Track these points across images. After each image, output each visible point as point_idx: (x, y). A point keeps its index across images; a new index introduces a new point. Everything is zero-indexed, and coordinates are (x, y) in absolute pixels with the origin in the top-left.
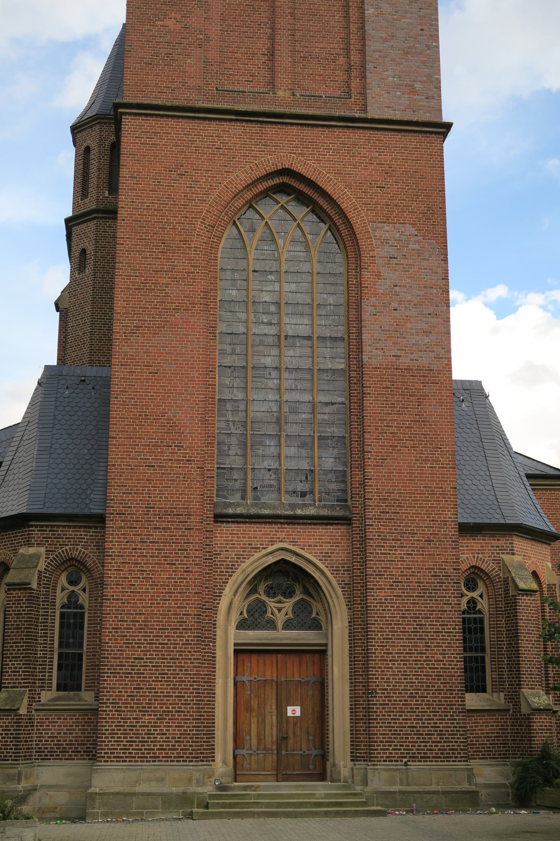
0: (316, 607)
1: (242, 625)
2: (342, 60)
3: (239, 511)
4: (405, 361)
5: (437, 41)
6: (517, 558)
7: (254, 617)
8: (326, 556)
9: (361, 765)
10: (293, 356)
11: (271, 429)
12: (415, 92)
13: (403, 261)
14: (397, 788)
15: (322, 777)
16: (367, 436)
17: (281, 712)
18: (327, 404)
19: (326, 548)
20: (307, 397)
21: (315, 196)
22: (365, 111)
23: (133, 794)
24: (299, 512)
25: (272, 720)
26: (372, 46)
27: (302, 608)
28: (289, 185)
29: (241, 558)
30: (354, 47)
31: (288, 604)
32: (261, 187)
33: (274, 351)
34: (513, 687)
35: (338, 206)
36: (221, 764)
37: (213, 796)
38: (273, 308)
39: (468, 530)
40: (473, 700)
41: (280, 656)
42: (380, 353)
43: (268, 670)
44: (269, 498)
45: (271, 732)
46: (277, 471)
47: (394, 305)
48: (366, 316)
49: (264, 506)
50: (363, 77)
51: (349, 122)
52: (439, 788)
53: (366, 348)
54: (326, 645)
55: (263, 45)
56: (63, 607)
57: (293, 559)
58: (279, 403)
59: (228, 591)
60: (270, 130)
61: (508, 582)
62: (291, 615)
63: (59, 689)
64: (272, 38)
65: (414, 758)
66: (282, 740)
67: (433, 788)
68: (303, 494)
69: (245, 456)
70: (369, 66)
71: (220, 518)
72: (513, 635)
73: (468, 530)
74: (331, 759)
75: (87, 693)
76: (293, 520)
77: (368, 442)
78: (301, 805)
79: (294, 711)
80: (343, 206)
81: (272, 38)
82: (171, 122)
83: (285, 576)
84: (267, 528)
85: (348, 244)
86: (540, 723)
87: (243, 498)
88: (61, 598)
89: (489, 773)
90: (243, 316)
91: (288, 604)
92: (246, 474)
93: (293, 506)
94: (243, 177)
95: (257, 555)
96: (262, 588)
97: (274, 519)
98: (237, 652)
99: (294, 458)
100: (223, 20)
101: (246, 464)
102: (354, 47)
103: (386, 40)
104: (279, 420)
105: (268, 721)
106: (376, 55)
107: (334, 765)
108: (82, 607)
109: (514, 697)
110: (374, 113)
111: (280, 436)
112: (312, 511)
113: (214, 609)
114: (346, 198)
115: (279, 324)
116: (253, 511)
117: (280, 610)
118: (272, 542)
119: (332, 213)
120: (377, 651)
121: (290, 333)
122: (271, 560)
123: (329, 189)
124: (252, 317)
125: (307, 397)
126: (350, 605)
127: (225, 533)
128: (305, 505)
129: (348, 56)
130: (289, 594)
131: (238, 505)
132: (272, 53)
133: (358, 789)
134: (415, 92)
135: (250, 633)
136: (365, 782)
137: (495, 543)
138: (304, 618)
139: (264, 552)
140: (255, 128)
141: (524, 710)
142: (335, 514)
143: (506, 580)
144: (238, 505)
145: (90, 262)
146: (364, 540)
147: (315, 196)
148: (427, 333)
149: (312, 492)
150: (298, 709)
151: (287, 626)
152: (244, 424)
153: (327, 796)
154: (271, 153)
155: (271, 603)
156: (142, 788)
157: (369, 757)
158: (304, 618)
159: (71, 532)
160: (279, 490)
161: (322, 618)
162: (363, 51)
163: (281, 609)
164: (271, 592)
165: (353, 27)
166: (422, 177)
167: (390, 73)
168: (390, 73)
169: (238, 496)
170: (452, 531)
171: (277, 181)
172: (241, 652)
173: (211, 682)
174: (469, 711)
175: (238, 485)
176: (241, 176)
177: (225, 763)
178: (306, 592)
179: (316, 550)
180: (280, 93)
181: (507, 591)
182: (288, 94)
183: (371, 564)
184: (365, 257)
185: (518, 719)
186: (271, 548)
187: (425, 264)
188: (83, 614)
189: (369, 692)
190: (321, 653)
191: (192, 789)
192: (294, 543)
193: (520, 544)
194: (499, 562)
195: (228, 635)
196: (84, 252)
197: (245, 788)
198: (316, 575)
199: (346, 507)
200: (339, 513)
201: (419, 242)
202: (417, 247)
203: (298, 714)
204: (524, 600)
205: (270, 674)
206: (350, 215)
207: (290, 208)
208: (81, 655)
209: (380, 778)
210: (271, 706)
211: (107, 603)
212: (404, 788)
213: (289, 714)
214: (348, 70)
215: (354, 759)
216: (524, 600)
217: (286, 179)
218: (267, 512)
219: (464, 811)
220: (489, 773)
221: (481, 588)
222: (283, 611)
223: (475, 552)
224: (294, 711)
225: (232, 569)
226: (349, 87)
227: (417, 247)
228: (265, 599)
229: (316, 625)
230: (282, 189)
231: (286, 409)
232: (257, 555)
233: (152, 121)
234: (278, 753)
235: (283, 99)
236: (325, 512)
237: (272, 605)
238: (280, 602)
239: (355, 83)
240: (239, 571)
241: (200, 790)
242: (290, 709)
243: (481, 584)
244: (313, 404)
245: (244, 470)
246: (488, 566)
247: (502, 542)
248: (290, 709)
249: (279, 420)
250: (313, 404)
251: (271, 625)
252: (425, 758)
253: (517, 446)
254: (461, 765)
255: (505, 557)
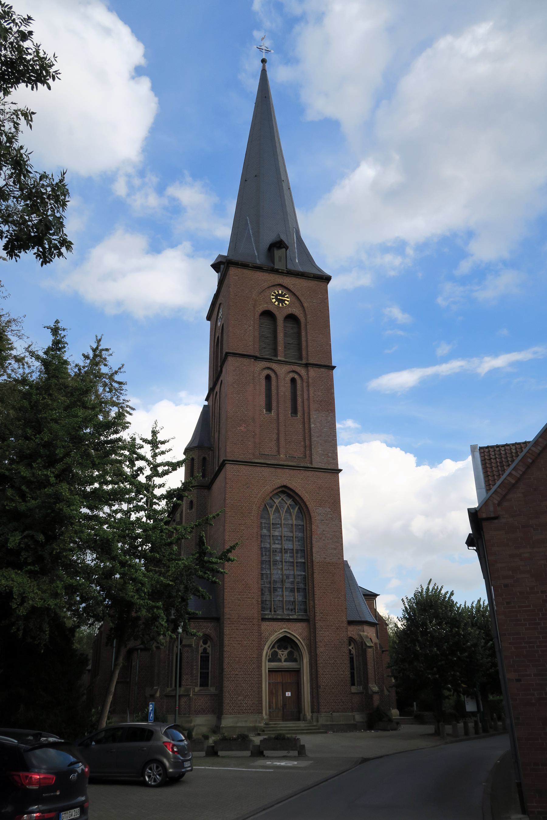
0: (296, 655)
1: (270, 661)
2: (302, 443)
3: (270, 617)
4: (328, 560)
5: (336, 437)
6: (365, 633)
7: (274, 658)
8: (300, 634)
9: (315, 714)
10: (287, 557)
11: (279, 585)
12: (329, 457)
13: (326, 522)
14: (329, 723)
15: (299, 719)
16: (315, 588)
17: (284, 694)
18: (299, 575)
19: (300, 631)
20: (292, 573)
21: (294, 495)
22: (311, 463)
23: (237, 727)
24: (291, 617)
25: (280, 698)
26: (314, 439)
27: (290, 654)
28: (286, 491)
29: (271, 635)
30: (307, 439)
31: (286, 652)
32: (275, 492)
33: (280, 554)
34: (365, 683)
35: (303, 500)
36: (265, 714)
37: (264, 727)
38: (279, 538)
39: (350, 623)
40: (354, 689)
41: (283, 673)
42: (319, 556)
43: (279, 678)
44: (279, 612)
45: (280, 703)
46: (282, 601)
47: (323, 538)
48: (314, 542)
49: (278, 615)
50: (311, 450)
51: (306, 468)
52: (343, 723)
53: (314, 555)
54: (300, 668)
55: (275, 436)
56: (201, 653)
57: (289, 635)
58: (282, 575)
59: (266, 647)
60: (279, 470)
61: (363, 643)
62: (287, 657)
63: (200, 686)
64: (278, 434)
65: (334, 712)
66: (284, 706)
67: (341, 723)
68: (292, 610)
69: (271, 595)
70: (313, 447)
71: (263, 619)
72: (365, 663)
73: (350, 623)
74: (303, 712)
75: (212, 688)
76: (289, 620)
77: (315, 591)
78: (297, 730)
79: (288, 694)
80: (305, 500)
81: (278, 434)
82: (244, 467)
83: (285, 642)
84: (279, 623)
85: (306, 514)
86: (376, 698)
87: (270, 611)
88: (201, 650)
89: (359, 717)
90: (268, 541)
91: (286, 652)
92: (271, 602)
93: (289, 615)
94: (269, 488)
95: (276, 634)
96: (276, 646)
97: (282, 620)
98: (269, 671)
99: (288, 596)
100: (260, 427)
101: (271, 598)
102: (307, 439)
103: (318, 437)
104: (282, 581)
105: (279, 697)
106: (315, 442)
107: (305, 715)
108: (208, 653)
109: (366, 687)
110: (315, 465)
111: (283, 588)
112: (295, 617)
113: (261, 655)
114: (306, 497)
115: (282, 544)
116: (275, 617)
117: (283, 654)
118: (281, 629)
119: (300, 502)
120: (320, 671)
121: (286, 548)
122: (281, 636)
123: (300, 493)
124: (272, 542)
125: (292, 573)
126: (310, 653)
127: (265, 625)
128: (292, 615)
129: (305, 442)
130: (286, 648)
131: (269, 614)
132: (278, 439)
133: (315, 723)
134: (329, 457)
135: (272, 664)
136: (318, 721)
137: (357, 628)
138: (291, 658)
139: (279, 633)
140: (273, 470)
141: (370, 692)
142: (304, 618)
143: (362, 642)
144: (269, 614)
145: (195, 506)
146: (315, 628)
147: (294, 495)
148: (335, 549)
149: (295, 609)
150: (290, 693)
151: (285, 661)
152: (270, 583)
153: (305, 726)
154: (279, 479)
155: (280, 652)
156: (239, 724)
157: (318, 711)
158: (291, 658)
159: (205, 624)
160: (283, 608)
161: (298, 658)
162: (310, 440)
163: (283, 654)
164: (279, 648)
165: (307, 431)
166: (332, 489)
167: (320, 449)
168: (320, 449)
169: (269, 610)
170: (345, 624)
171: (281, 489)
172: (271, 671)
173: (261, 683)
174: (352, 693)
175: (268, 606)
176: (269, 488)
177: (266, 714)
178: (292, 647)
179: (297, 632)
180: (282, 456)
181: (362, 647)
182: (284, 456)
183: (317, 638)
184: (313, 520)
185: (367, 695)
186: (281, 631)
187: (334, 522)
188: (208, 657)
189: (318, 687)
190: (297, 672)
191: (257, 725)
192: (289, 629)
193: (366, 628)
194: (361, 637)
195: (266, 666)
196: (192, 502)
197: (275, 724)
198: (297, 642)
199: (307, 615)
200: (305, 618)
201: (331, 514)
202: (331, 516)
203: (290, 695)
204: (369, 650)
205: (279, 680)
206: (307, 504)
207: (284, 499)
208: (208, 673)
209: (323, 720)
210: (280, 692)
211: (225, 653)
212: (331, 723)
213: (287, 695)
214: (305, 447)
215: (312, 712)
216: (369, 650)
217: (284, 489)
218: (279, 617)
219: (353, 731)
220: (359, 717)
221: (352, 646)
222: (284, 655)
223: (353, 631)
224: (288, 694)
225: (267, 639)
226: (305, 453)
227: (331, 516)
228: (277, 650)
229: (295, 660)
230: (283, 492)
231: (285, 577)
232: (276, 634)
233: (237, 466)
234: (283, 711)
235: (282, 459)
236: (300, 617)
237: (280, 653)
238: (283, 651)
239: (308, 452)
240: (270, 640)
241: (260, 725)
242: (287, 693)
243: (352, 644)
244: (294, 575)
245: (271, 601)
246: (356, 637)
247: (360, 628)
248: (287, 693)
249: (282, 581)
250: (294, 575)
251: (280, 660)
252: (338, 712)
253: (360, 584)
254: (350, 714)
255: (361, 633)
